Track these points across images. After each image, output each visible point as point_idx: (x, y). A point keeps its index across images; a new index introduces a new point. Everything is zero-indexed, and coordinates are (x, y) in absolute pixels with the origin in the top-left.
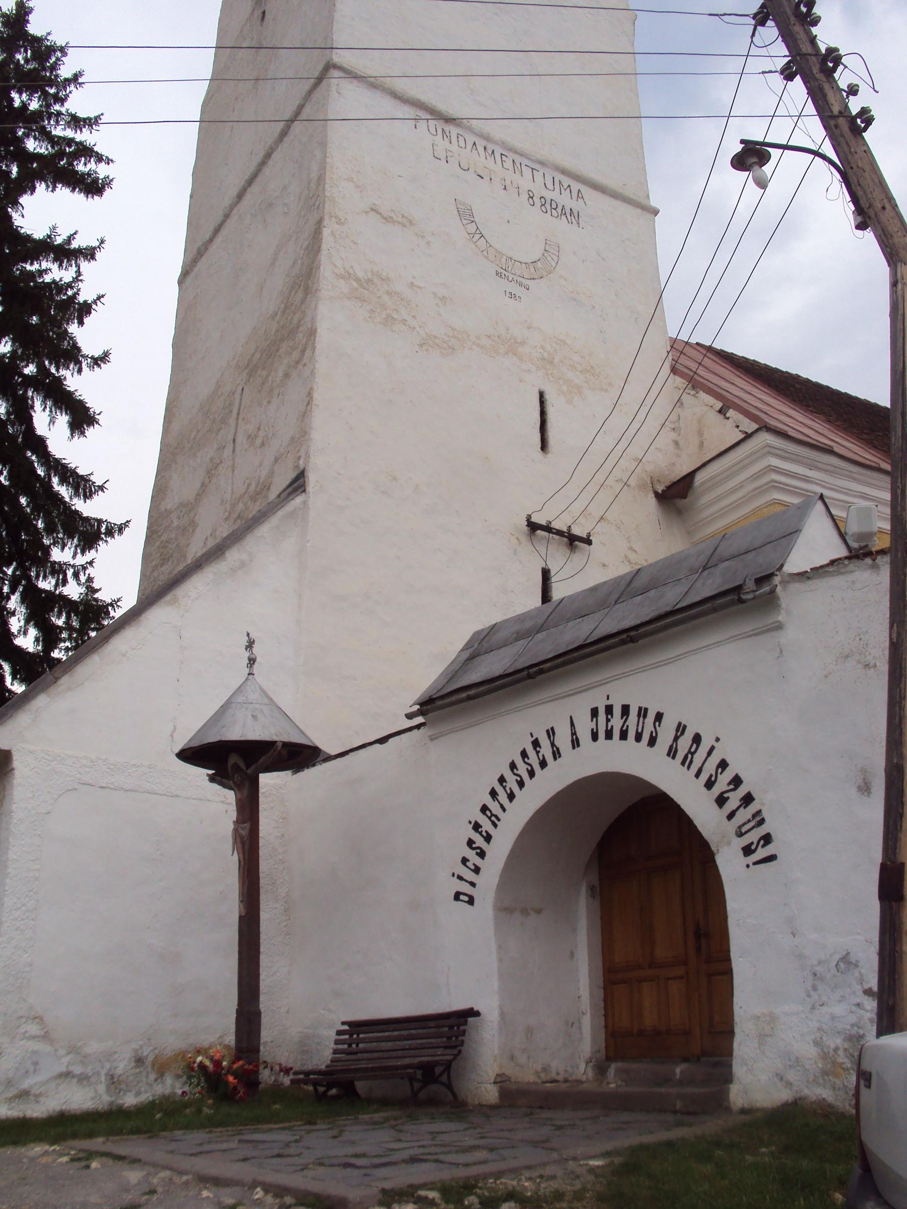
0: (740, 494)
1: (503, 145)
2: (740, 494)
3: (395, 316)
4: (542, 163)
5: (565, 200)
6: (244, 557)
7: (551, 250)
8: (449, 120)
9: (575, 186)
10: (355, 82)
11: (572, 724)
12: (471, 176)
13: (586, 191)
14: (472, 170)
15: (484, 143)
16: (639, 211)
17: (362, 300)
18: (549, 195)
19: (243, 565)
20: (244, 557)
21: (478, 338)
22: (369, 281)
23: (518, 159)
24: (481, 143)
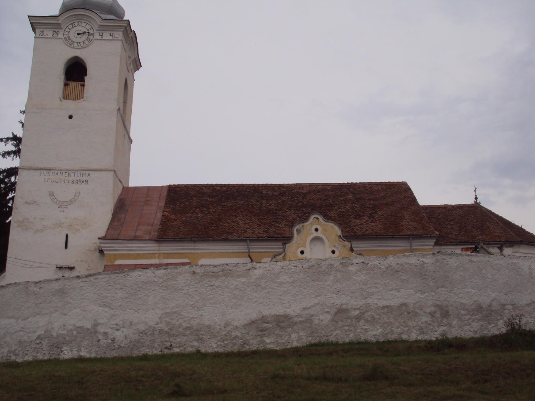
4: (77, 171)
5: (84, 178)
7: (77, 194)
8: (50, 170)
9: (87, 173)
13: (90, 172)
23: (70, 172)
24: (59, 172)
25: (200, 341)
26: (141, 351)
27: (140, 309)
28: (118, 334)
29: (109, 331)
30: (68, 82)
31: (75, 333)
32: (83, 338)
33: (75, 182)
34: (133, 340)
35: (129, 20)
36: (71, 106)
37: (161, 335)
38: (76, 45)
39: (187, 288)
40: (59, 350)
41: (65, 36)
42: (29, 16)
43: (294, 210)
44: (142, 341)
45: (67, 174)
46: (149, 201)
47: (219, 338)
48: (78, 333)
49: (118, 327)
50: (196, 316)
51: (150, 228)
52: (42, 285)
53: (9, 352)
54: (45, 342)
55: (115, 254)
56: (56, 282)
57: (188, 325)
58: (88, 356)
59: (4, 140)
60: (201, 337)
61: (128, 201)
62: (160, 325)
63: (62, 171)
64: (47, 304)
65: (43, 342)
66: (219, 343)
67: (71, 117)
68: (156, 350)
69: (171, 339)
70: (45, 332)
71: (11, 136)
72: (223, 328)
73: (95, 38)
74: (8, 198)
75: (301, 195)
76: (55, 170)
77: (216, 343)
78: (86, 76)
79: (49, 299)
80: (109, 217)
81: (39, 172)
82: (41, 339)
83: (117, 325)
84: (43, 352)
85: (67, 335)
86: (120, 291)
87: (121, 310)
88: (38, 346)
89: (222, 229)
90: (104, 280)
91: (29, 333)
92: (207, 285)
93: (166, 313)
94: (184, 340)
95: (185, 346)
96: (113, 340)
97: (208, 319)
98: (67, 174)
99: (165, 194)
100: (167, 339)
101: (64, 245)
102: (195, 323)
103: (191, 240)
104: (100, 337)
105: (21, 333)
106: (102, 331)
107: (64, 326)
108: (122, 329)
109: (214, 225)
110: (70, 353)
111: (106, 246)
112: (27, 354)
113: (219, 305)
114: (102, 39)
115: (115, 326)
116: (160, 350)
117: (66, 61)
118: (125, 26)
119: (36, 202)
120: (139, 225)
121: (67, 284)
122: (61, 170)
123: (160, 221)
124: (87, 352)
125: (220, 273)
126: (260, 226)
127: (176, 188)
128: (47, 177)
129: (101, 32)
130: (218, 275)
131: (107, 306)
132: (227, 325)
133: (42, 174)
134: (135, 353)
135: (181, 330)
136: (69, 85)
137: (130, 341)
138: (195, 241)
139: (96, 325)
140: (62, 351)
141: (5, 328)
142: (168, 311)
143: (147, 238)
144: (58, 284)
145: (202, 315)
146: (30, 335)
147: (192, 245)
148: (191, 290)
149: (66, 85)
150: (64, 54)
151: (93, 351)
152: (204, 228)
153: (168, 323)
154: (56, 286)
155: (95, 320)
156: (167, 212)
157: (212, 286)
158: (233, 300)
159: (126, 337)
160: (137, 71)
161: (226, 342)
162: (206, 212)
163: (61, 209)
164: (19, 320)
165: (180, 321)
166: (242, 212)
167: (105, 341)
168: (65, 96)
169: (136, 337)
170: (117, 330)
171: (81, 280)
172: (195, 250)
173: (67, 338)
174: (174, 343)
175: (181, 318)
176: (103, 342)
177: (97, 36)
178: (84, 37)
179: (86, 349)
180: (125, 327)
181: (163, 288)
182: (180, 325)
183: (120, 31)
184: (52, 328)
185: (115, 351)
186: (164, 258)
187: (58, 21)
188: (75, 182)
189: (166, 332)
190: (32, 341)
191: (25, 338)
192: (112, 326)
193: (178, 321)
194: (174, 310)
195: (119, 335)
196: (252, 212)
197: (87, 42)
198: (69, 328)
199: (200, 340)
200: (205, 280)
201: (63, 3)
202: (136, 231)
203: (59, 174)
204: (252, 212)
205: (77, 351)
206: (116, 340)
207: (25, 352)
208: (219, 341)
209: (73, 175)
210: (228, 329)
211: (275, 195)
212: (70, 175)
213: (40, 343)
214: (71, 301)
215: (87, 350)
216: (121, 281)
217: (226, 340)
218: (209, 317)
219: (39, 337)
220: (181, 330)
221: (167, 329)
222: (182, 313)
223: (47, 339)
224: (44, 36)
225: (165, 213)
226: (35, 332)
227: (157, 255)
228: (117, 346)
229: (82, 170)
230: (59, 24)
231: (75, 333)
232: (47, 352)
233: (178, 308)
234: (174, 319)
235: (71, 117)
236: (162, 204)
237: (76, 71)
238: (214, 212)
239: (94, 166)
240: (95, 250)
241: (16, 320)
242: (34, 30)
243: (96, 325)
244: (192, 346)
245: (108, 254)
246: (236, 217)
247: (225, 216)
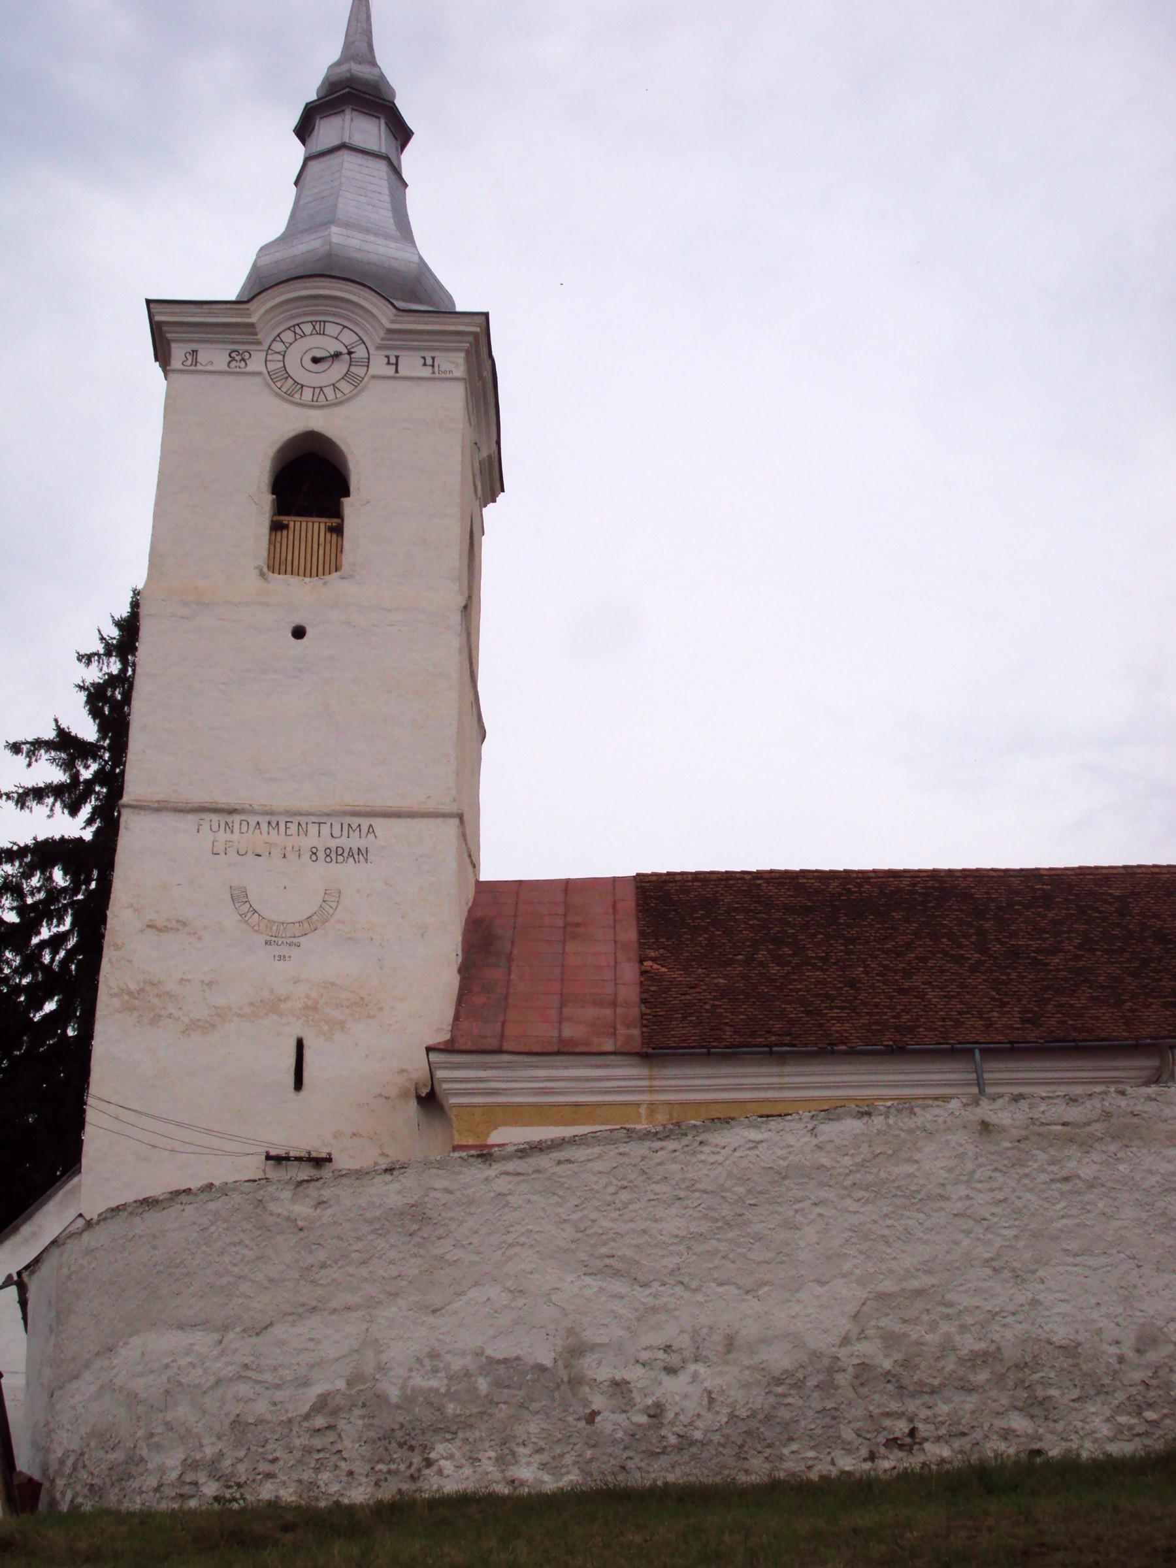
0: (464, 1086)
1: (287, 813)
2: (464, 1086)
3: (162, 1013)
4: (328, 815)
5: (355, 842)
6: (35, 1228)
7: (331, 897)
8: (232, 812)
9: (365, 822)
10: (142, 812)
11: (25, 1318)
12: (251, 857)
13: (377, 823)
14: (250, 852)
15: (268, 818)
16: (439, 820)
17: (131, 1009)
18: (333, 844)
19: (34, 1234)
20: (35, 1228)
21: (241, 1009)
22: (142, 990)
23: (303, 820)
24: (264, 820)
25: (1036, 1411)
26: (781, 1458)
27: (763, 1284)
28: (674, 1386)
29: (635, 1375)
30: (285, 519)
31: (483, 1384)
32: (522, 1406)
33: (321, 855)
34: (743, 1413)
36: (299, 595)
37: (864, 1391)
38: (307, 395)
39: (963, 1191)
40: (417, 1460)
41: (271, 366)
42: (148, 302)
43: (1105, 951)
44: (784, 1413)
45: (293, 828)
46: (578, 925)
47: (1120, 1397)
48: (499, 1384)
49: (674, 1360)
50: (1011, 1307)
51: (608, 1012)
52: (326, 1194)
53: (191, 1465)
54: (352, 1427)
56: (388, 1177)
57: (980, 1346)
58: (550, 1484)
59: (25, 748)
60: (1040, 1393)
61: (505, 929)
62: (862, 1347)
63: (273, 817)
64: (351, 1269)
65: (342, 1424)
66: (1123, 1419)
67: (299, 633)
68: (849, 1452)
69: (912, 1406)
70: (350, 1383)
71: (50, 734)
72: (1131, 1354)
73: (372, 372)
74: (35, 940)
75: (1111, 904)
76: (254, 812)
77: (1108, 1420)
79: (359, 1246)
80: (449, 980)
82: (335, 1412)
83: (667, 1349)
84: (343, 1464)
85: (448, 1394)
86: (673, 1211)
87: (679, 1290)
88: (317, 1442)
89: (870, 1014)
90: (597, 1166)
91: (277, 1387)
92: (1043, 1177)
93: (881, 1296)
94: (969, 1407)
95: (977, 1435)
96: (656, 1413)
97: (1065, 1315)
98: (293, 828)
99: (629, 903)
100: (894, 1406)
102: (1009, 1334)
103: (771, 1053)
104: (598, 1401)
105: (243, 1389)
106: (603, 1374)
107: (434, 1355)
108: (692, 1367)
109: (838, 1003)
110: (467, 1471)
111: (456, 1078)
112: (269, 1476)
113: (1103, 1260)
114: (396, 377)
115: (661, 1355)
116: (864, 1452)
117: (276, 447)
118: (476, 335)
119: (185, 924)
120: (562, 1005)
121: (440, 1183)
122: (272, 813)
123: (637, 989)
124: (543, 1466)
125: (1098, 1128)
126: (1003, 1004)
127: (665, 882)
128: (222, 836)
129: (392, 354)
130: (1091, 1135)
131: (617, 1274)
132: (1146, 1341)
133: (205, 827)
134: (756, 1470)
135: (950, 1364)
136: (286, 527)
137: (732, 1416)
138: (781, 1058)
139: (576, 1350)
140: (429, 1463)
141: (167, 1366)
142: (888, 1286)
143: (609, 1046)
144: (397, 1186)
145: (1034, 1303)
146: (279, 1395)
147: (775, 1070)
148: (980, 1198)
149: (277, 527)
150: (266, 423)
151: (569, 1459)
152: (808, 1013)
153: (891, 1340)
154: (389, 1194)
155: (571, 1331)
156: (653, 960)
157: (1066, 1179)
158: (1161, 1238)
159: (712, 1400)
160: (491, 505)
161: (1150, 1415)
162: (796, 960)
163: (277, 951)
164: (231, 1335)
165: (945, 1327)
166: (922, 959)
167: (621, 1418)
168: (277, 564)
169: (759, 1400)
170: (671, 1370)
171: (497, 1168)
173: (451, 1408)
174: (926, 1420)
175: (948, 1317)
176: (611, 1422)
177: (379, 366)
178: (337, 370)
179: (540, 1450)
180: (705, 1360)
181: (861, 1193)
182: (947, 1347)
183: (455, 350)
184: (381, 1368)
185: (664, 1461)
187: (249, 316)
188: (321, 855)
189: (888, 1376)
190: (290, 1421)
191: (262, 1407)
192: (645, 1356)
193: (933, 1327)
194: (915, 1284)
195: (678, 1391)
196: (959, 960)
197: (345, 387)
198: (457, 1364)
199: (1038, 1406)
200: (1034, 1158)
201: (255, 267)
202: (560, 1023)
203: (264, 826)
204: (959, 960)
205: (500, 1461)
206: (670, 1415)
207: (264, 1467)
208: (1119, 1409)
210: (1152, 1356)
211: (1019, 903)
212: (302, 830)
213: (330, 1427)
214: (458, 1253)
215: (545, 1457)
216: (674, 1167)
217: (1150, 1406)
218: (1066, 1308)
219: (322, 1404)
220: (950, 1364)
221: (887, 1364)
222: (948, 1296)
223: (357, 1412)
224: (199, 367)
225: (648, 963)
226: (306, 1383)
227: (643, 1110)
228: (673, 1440)
229: (345, 814)
230: (252, 325)
231: (483, 1384)
232: (360, 1467)
233: (928, 1272)
234: (916, 1321)
235: (299, 633)
236: (629, 934)
237: (310, 483)
238: (825, 960)
239: (389, 800)
240: (404, 1095)
241: (216, 1336)
242: (162, 354)
243: (576, 1350)
244: (1006, 1434)
245: (461, 1106)
246: (907, 974)
247: (866, 973)
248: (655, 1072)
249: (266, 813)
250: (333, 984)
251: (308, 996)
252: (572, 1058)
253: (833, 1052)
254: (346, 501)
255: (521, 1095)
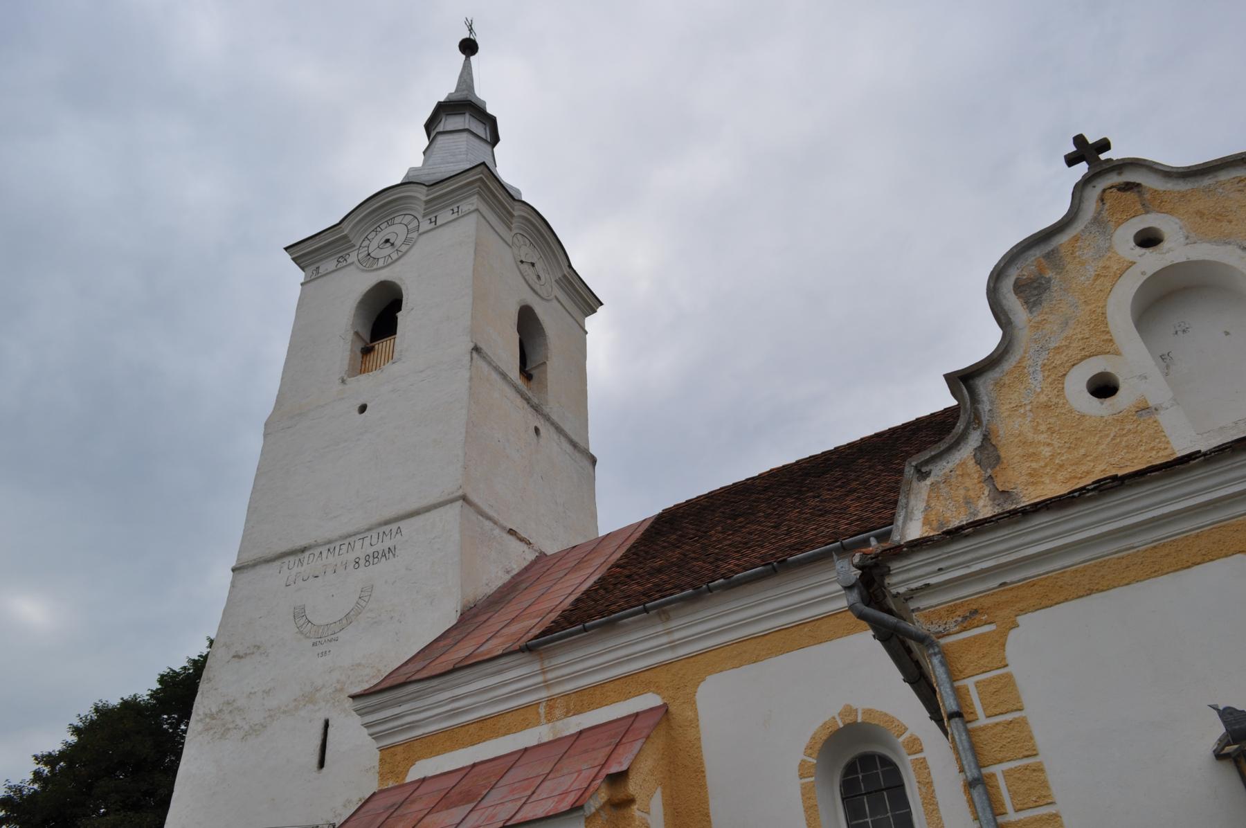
3: (231, 726)
4: (369, 530)
5: (388, 543)
8: (303, 550)
9: (394, 527)
13: (402, 524)
18: (370, 551)
23: (351, 540)
24: (324, 549)
33: (362, 562)
35: (484, 163)
42: (286, 249)
55: (408, 744)
67: (363, 409)
78: (400, 309)
81: (277, 563)
101: (315, 760)
118: (481, 179)
119: (259, 647)
122: (330, 542)
129: (432, 217)
150: (352, 284)
172: (673, 646)
186: (568, 713)
188: (362, 562)
209: (358, 544)
227: (542, 710)
230: (345, 237)
248: (546, 664)
249: (325, 544)
250: (359, 665)
251: (338, 682)
252: (468, 671)
253: (710, 590)
254: (399, 315)
255: (496, 734)
